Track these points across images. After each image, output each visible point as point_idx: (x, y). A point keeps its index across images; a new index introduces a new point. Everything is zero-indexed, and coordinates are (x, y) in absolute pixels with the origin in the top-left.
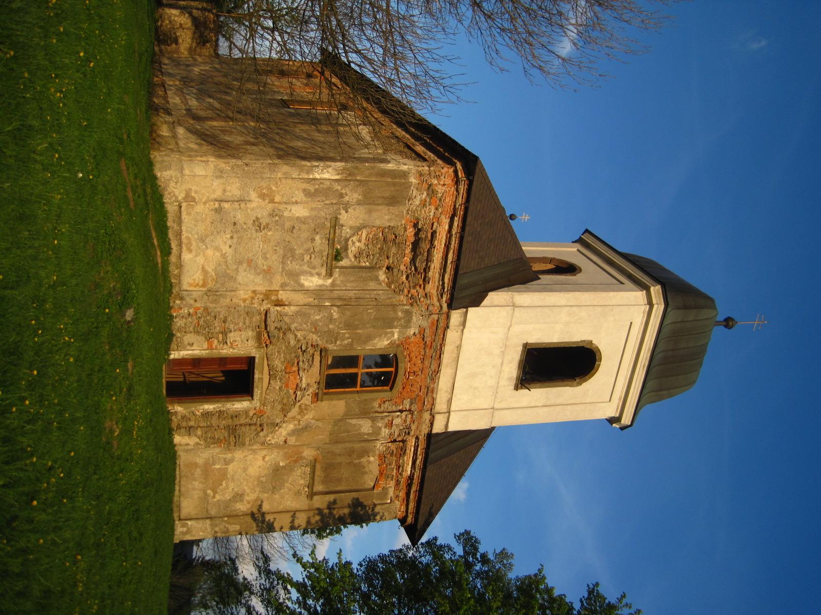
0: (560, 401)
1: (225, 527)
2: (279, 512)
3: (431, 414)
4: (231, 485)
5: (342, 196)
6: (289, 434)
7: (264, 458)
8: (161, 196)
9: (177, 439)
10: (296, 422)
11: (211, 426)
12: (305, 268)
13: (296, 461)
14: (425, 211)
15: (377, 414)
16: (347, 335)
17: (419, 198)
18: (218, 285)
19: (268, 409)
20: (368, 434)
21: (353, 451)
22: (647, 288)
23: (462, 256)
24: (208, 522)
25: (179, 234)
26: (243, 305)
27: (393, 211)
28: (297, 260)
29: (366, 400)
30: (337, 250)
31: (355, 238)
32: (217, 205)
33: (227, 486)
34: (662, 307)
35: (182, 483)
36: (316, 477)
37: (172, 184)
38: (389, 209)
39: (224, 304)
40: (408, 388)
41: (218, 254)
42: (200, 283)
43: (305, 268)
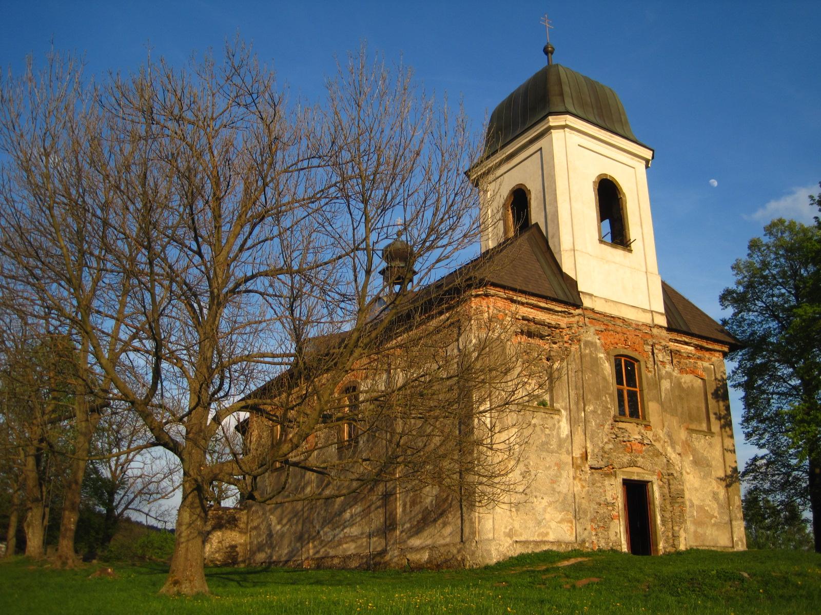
2: (724, 462)
4: (707, 502)
6: (674, 451)
7: (688, 473)
8: (512, 558)
9: (682, 547)
10: (666, 445)
11: (672, 518)
12: (555, 433)
13: (689, 446)
19: (658, 469)
22: (550, 128)
23: (545, 294)
24: (734, 523)
25: (537, 543)
26: (587, 488)
30: (539, 404)
33: (709, 505)
34: (568, 117)
35: (708, 544)
36: (697, 429)
37: (501, 549)
39: (587, 504)
40: (637, 346)
41: (549, 509)
42: (570, 525)
43: (555, 433)
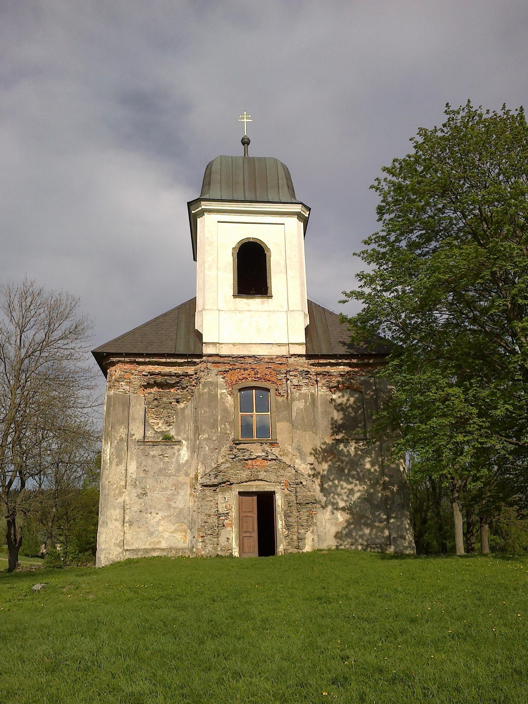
0: (283, 263)
1: (397, 507)
3: (290, 357)
5: (122, 440)
6: (304, 463)
9: (308, 549)
12: (174, 460)
14: (135, 381)
15: (289, 398)
16: (223, 426)
17: (124, 387)
18: (186, 521)
19: (283, 479)
20: (306, 402)
21: (326, 411)
25: (146, 551)
27: (134, 403)
28: (168, 466)
29: (276, 407)
31: (156, 427)
32: (127, 525)
37: (111, 557)
38: (132, 406)
42: (184, 534)
